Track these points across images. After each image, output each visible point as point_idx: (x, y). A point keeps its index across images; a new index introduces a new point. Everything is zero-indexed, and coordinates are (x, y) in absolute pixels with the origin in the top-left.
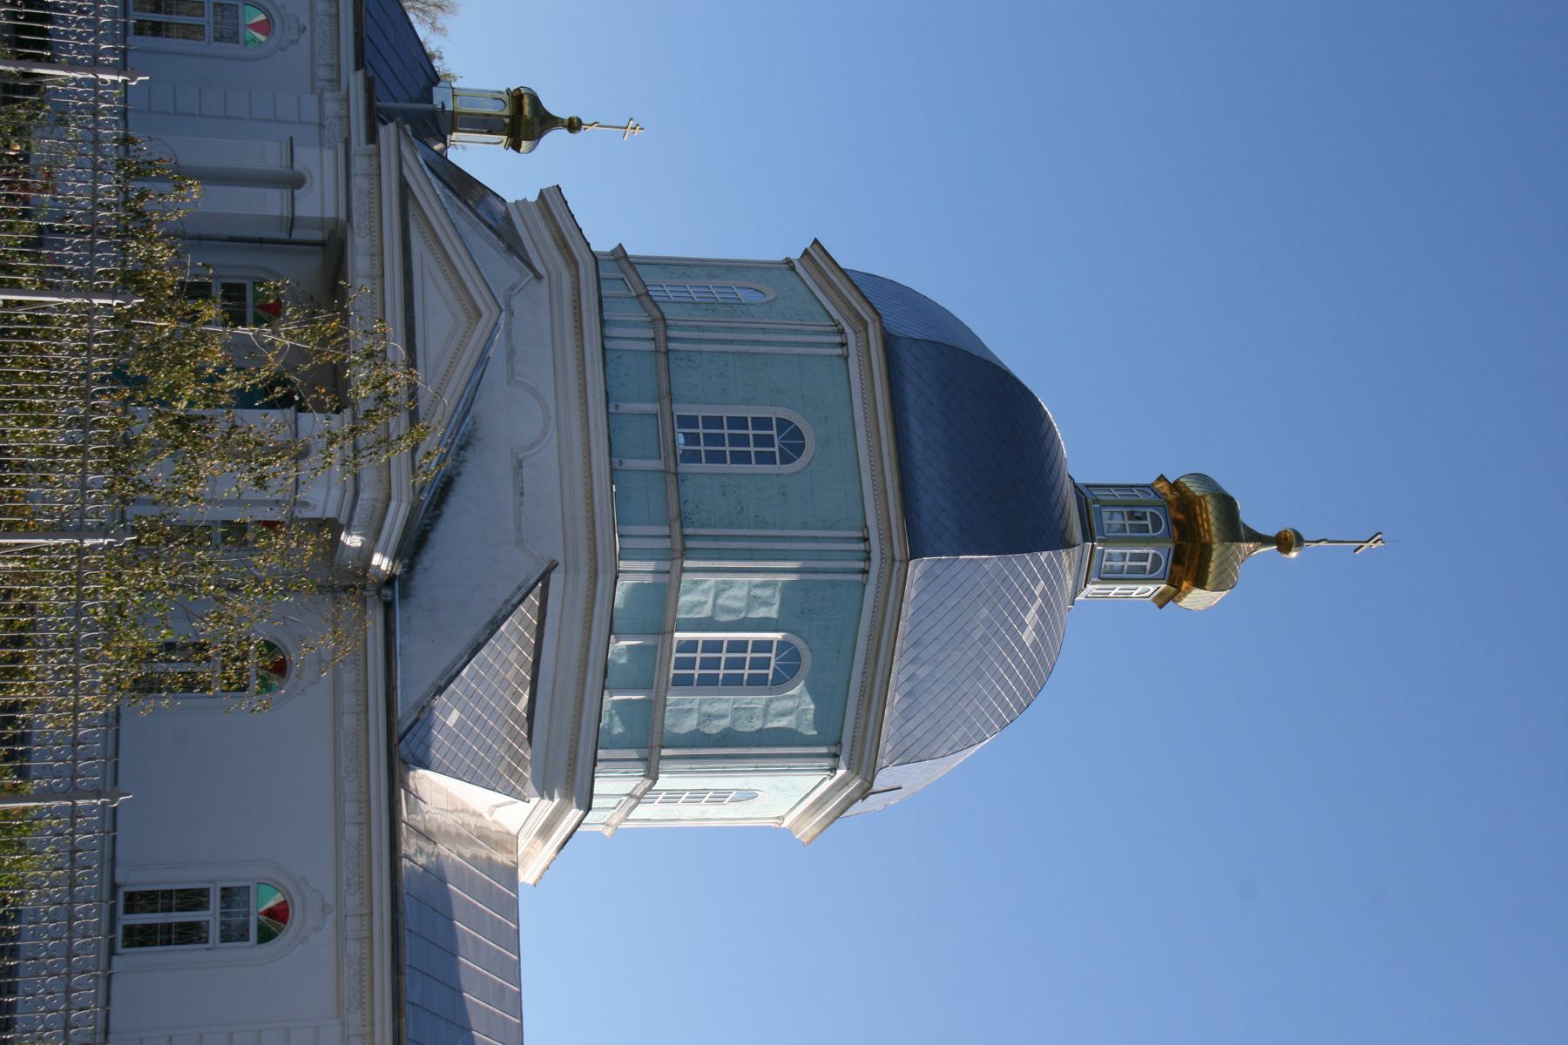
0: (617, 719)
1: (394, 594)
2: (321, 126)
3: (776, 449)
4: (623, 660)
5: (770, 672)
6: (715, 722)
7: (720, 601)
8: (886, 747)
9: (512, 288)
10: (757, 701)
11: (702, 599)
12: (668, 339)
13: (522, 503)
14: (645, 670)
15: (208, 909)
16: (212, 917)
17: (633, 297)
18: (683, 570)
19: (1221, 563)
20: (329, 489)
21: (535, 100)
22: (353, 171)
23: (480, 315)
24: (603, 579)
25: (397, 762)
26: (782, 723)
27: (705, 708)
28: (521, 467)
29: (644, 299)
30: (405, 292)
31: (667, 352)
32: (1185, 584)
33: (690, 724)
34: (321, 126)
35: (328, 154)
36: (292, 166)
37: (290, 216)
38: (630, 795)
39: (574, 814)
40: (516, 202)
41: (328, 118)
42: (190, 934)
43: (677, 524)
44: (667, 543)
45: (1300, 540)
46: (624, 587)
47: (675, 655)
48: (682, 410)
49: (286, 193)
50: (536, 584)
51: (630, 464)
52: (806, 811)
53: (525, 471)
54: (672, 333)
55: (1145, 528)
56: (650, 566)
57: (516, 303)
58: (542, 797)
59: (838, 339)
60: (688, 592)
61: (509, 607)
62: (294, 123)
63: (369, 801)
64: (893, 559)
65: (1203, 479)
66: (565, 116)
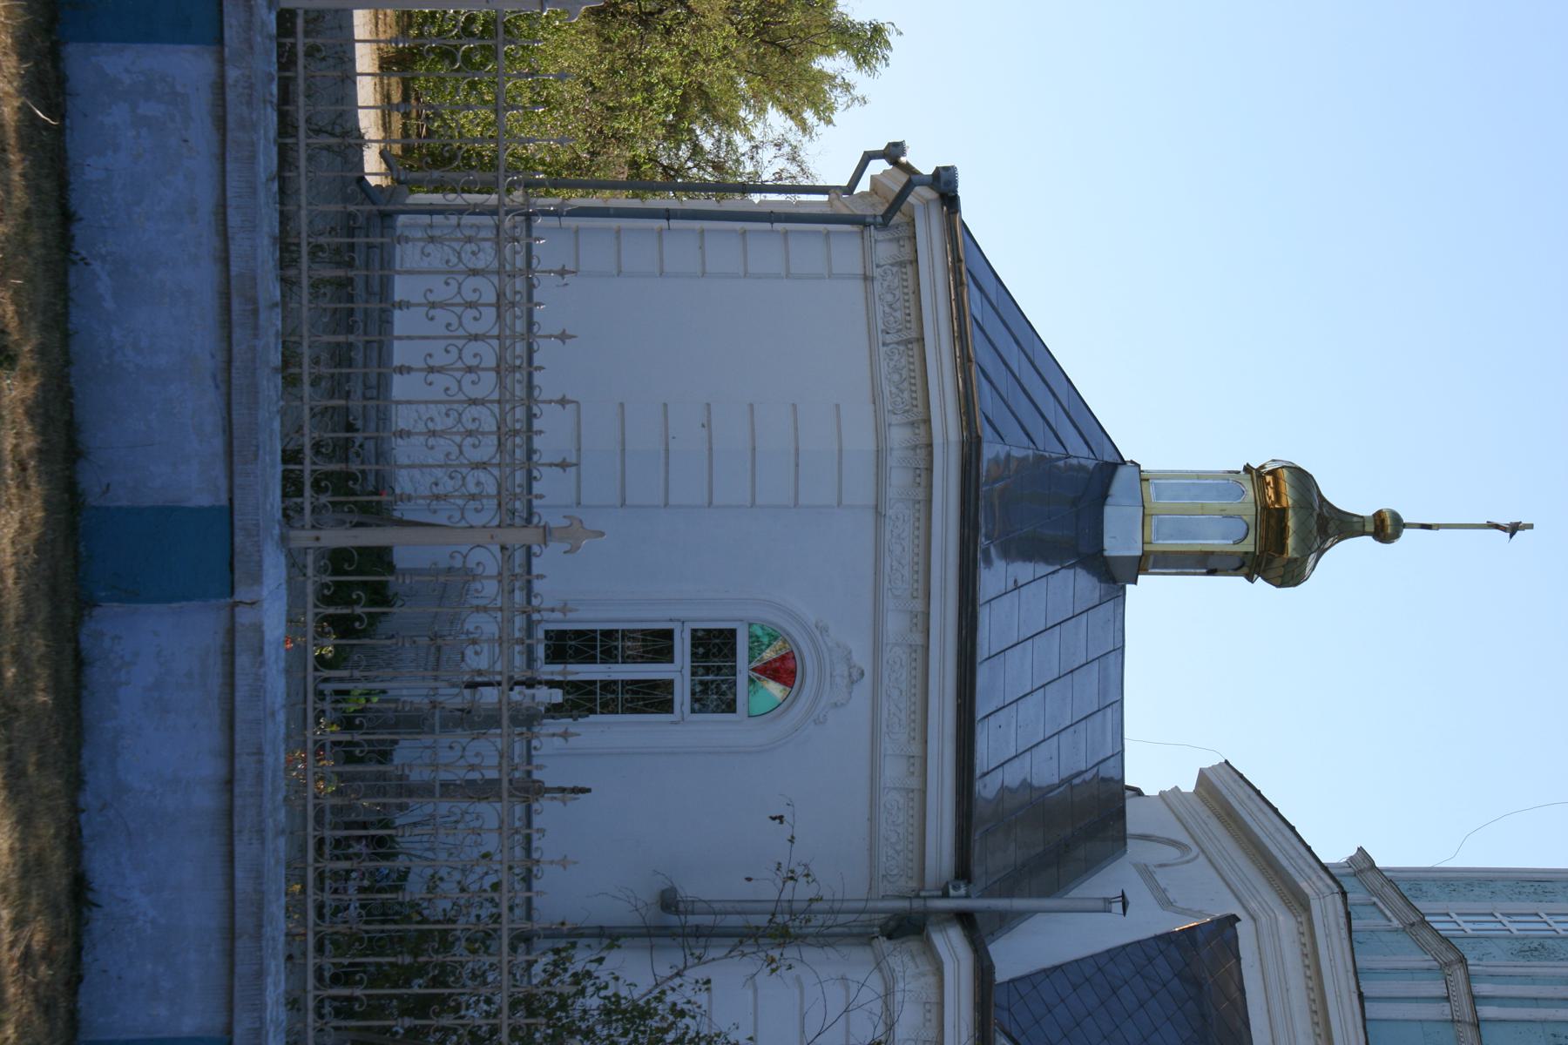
12: (1474, 999)
16: (678, 671)
17: (1396, 930)
31: (1477, 1024)
40: (1162, 794)
42: (654, 698)
54: (1482, 988)
66: (1367, 510)
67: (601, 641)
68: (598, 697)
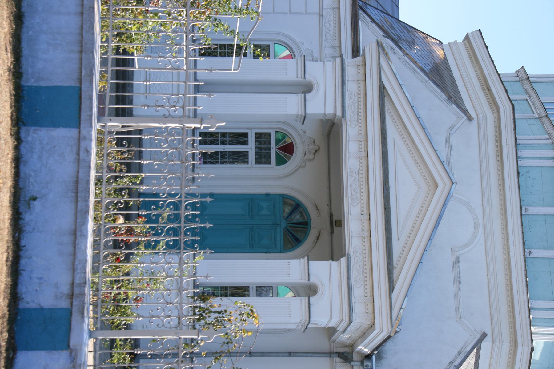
1: (372, 365)
2: (321, 15)
9: (451, 128)
13: (459, 289)
15: (248, 145)
16: (250, 148)
17: (536, 118)
22: (346, 78)
23: (437, 186)
28: (459, 262)
29: (545, 120)
30: (382, 146)
34: (321, 15)
35: (329, 65)
37: (303, 114)
40: (449, 44)
41: (325, 9)
49: (301, 96)
51: (537, 253)
53: (461, 264)
57: (454, 140)
62: (301, 14)
67: (221, 159)
68: (220, 160)
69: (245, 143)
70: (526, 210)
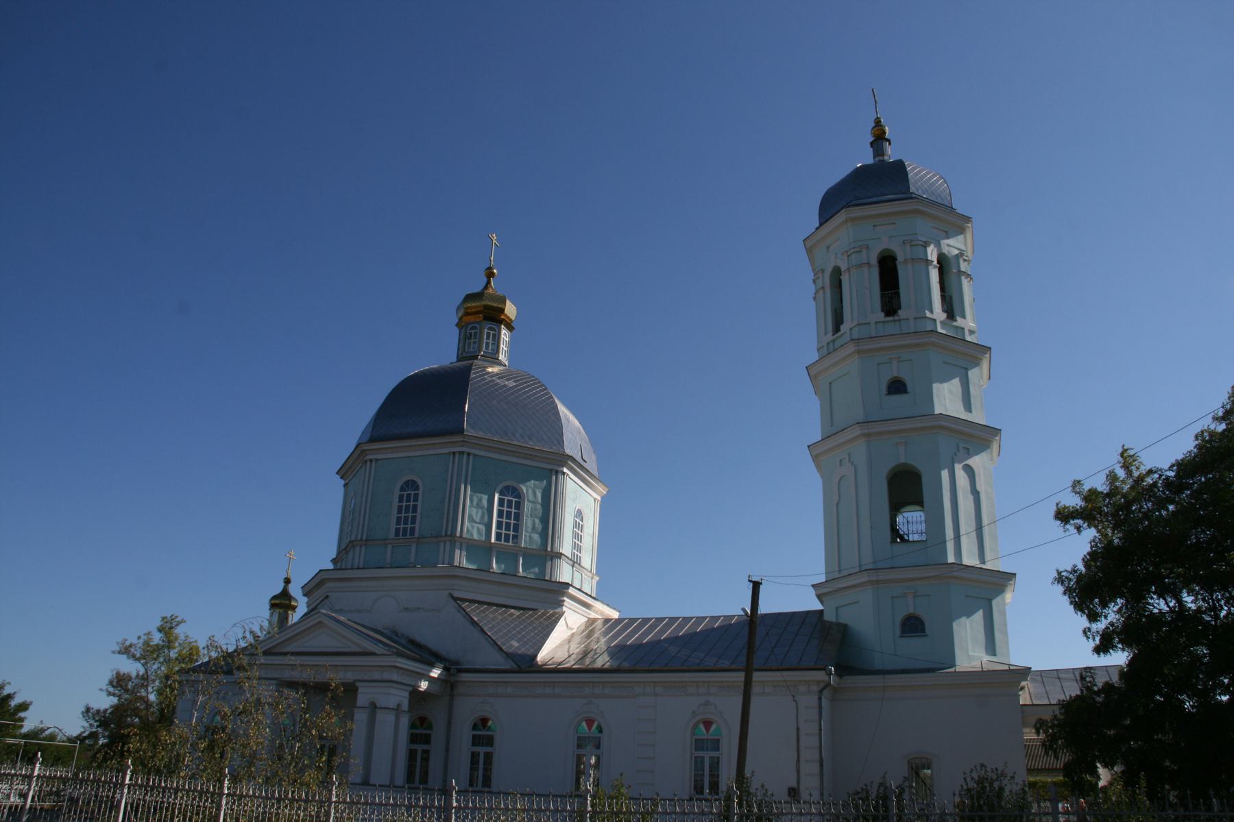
0: (531, 570)
3: (413, 493)
4: (503, 566)
5: (514, 499)
6: (537, 526)
7: (478, 521)
8: (554, 450)
10: (527, 507)
11: (476, 528)
12: (361, 539)
14: (509, 557)
18: (461, 537)
19: (493, 301)
20: (390, 694)
21: (274, 598)
24: (458, 572)
25: (532, 669)
26: (539, 495)
27: (529, 530)
31: (367, 540)
32: (503, 317)
33: (536, 537)
36: (366, 707)
38: (573, 566)
39: (571, 591)
43: (440, 539)
44: (448, 543)
45: (490, 268)
46: (468, 564)
47: (503, 542)
48: (392, 534)
49: (378, 711)
50: (457, 603)
52: (591, 488)
54: (359, 538)
55: (476, 333)
56: (457, 552)
58: (563, 605)
59: (368, 463)
60: (472, 535)
61: (467, 616)
63: (545, 682)
64: (463, 441)
65: (458, 309)
69: (416, 750)
70: (412, 563)
